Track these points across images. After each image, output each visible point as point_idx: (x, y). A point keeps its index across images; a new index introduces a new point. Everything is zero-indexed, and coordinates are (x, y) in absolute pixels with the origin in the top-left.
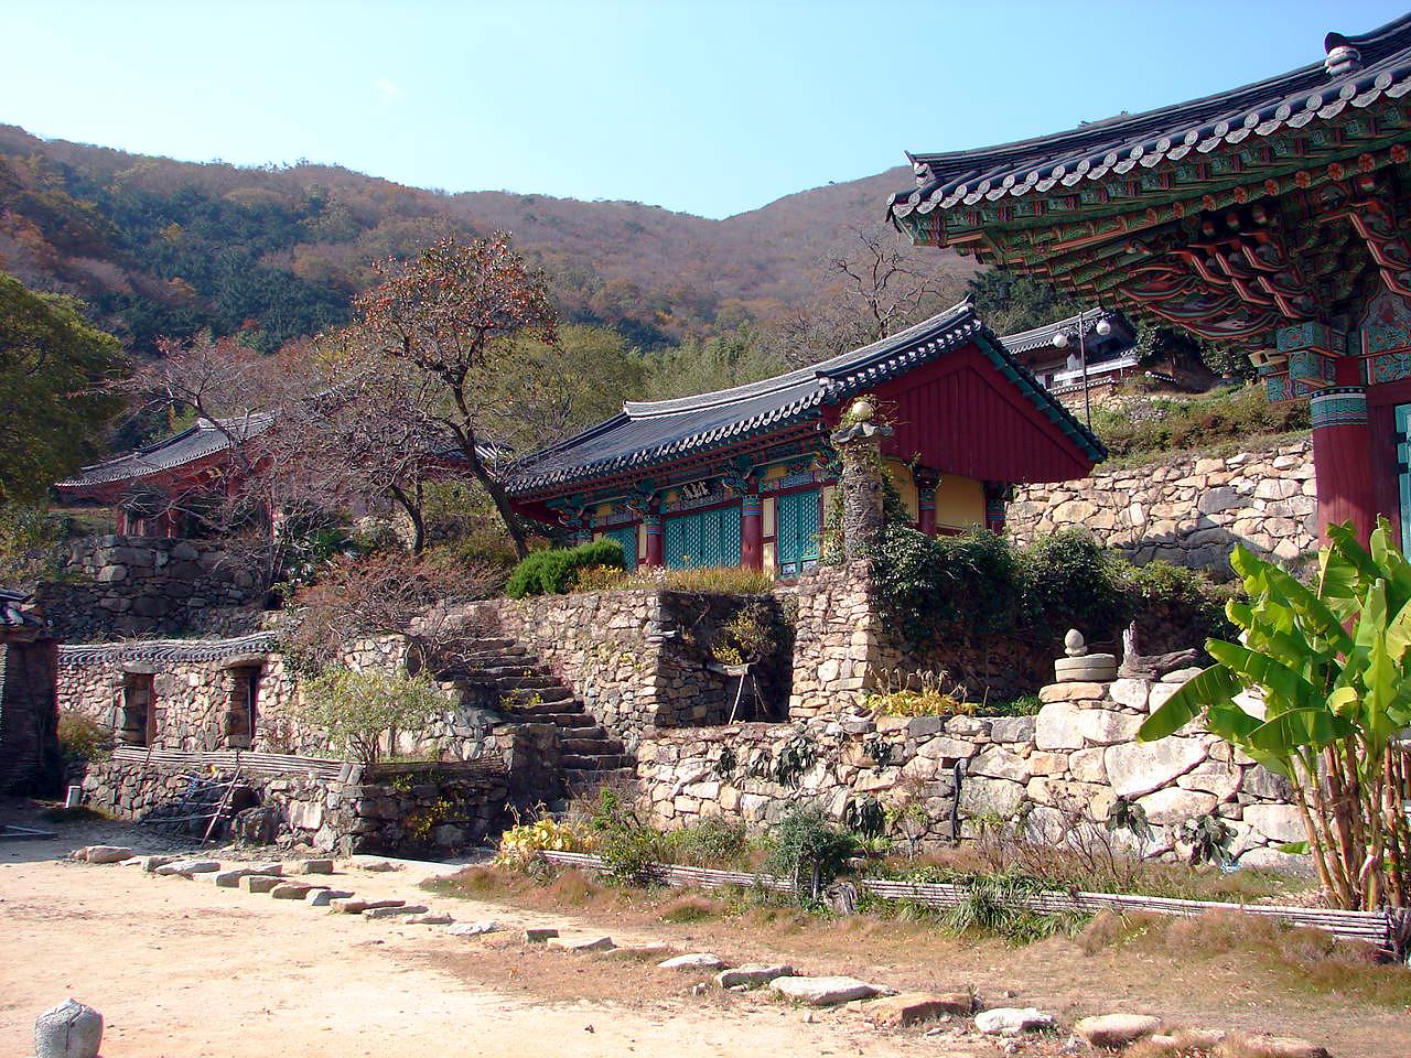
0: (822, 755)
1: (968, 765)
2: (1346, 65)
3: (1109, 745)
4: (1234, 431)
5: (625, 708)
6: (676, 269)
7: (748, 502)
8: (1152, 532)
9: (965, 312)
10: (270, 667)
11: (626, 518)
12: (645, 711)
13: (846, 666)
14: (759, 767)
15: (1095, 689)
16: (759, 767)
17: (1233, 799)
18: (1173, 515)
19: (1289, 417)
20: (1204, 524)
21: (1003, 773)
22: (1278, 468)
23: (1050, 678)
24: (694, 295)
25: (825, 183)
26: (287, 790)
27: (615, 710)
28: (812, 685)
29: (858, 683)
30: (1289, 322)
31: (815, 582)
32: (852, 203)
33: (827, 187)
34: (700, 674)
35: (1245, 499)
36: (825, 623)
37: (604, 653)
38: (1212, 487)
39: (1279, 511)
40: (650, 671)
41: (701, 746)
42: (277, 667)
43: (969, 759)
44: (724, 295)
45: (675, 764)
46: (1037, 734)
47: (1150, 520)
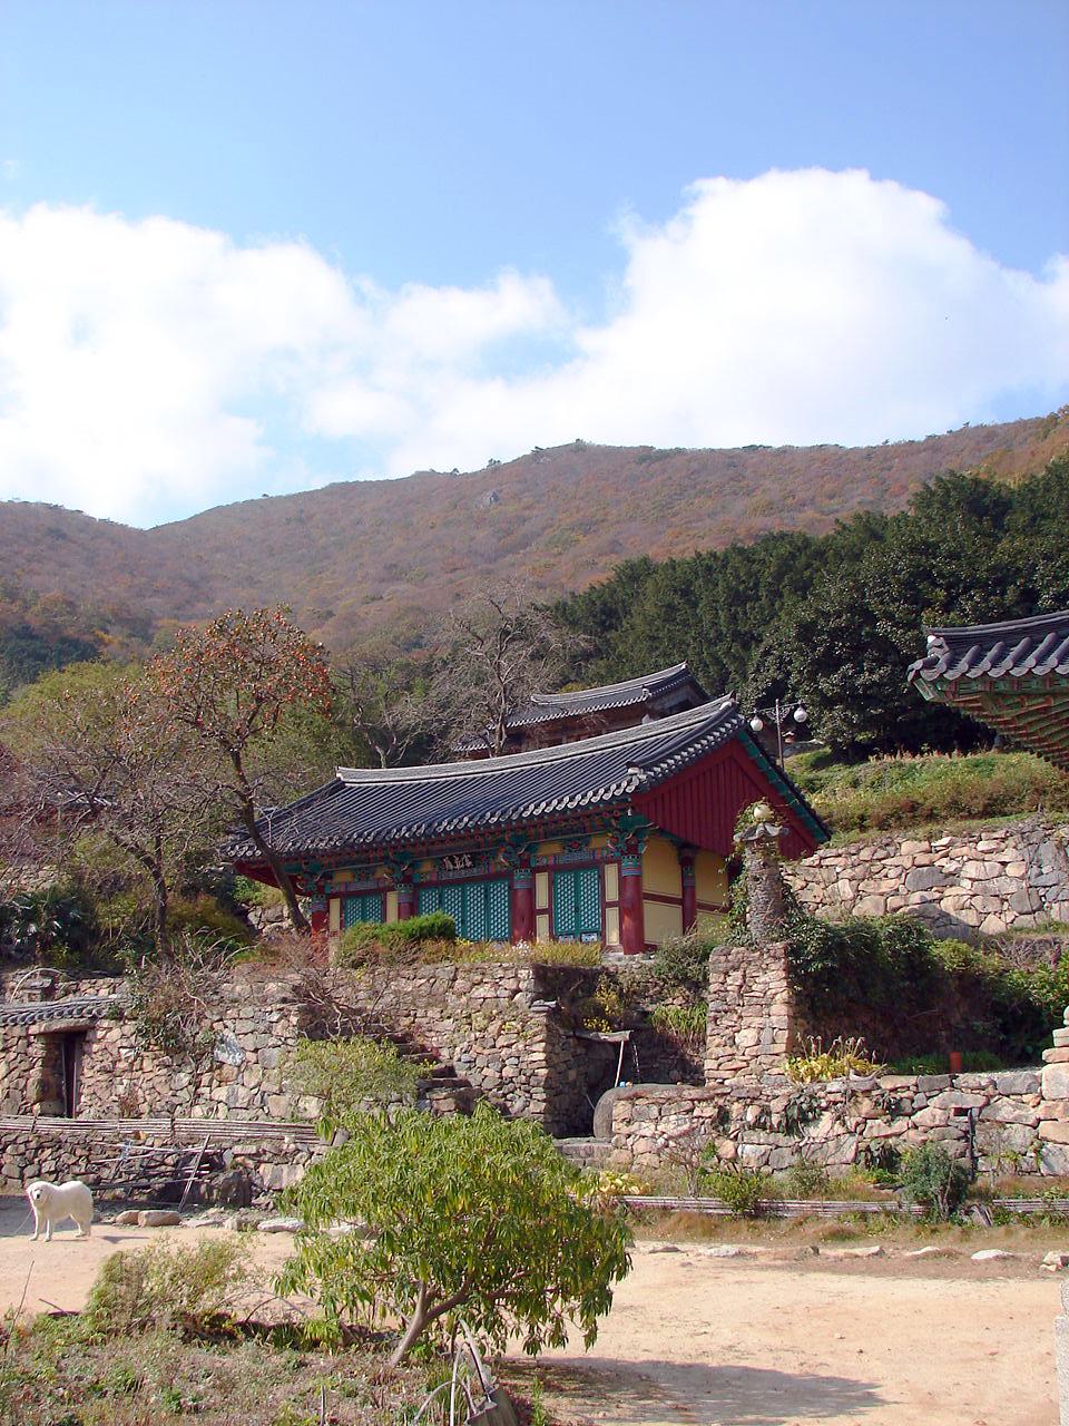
0: (826, 1109)
1: (980, 1113)
4: (931, 816)
5: (508, 1072)
6: (105, 583)
7: (520, 876)
9: (728, 708)
10: (100, 1034)
11: (370, 885)
12: (533, 1074)
13: (766, 1035)
14: (762, 1120)
16: (762, 1120)
18: (881, 891)
19: (986, 806)
21: (1015, 1118)
22: (982, 852)
23: (1051, 1045)
24: (128, 611)
25: (258, 496)
26: (257, 1154)
27: (498, 1075)
28: (729, 1050)
29: (780, 1048)
32: (289, 521)
33: (261, 500)
34: (571, 1040)
35: (952, 878)
36: (741, 996)
37: (479, 1021)
38: (918, 867)
39: (985, 889)
40: (538, 1038)
41: (688, 1105)
42: (113, 1037)
43: (981, 1109)
44: (158, 614)
45: (657, 1121)
46: (1044, 1087)
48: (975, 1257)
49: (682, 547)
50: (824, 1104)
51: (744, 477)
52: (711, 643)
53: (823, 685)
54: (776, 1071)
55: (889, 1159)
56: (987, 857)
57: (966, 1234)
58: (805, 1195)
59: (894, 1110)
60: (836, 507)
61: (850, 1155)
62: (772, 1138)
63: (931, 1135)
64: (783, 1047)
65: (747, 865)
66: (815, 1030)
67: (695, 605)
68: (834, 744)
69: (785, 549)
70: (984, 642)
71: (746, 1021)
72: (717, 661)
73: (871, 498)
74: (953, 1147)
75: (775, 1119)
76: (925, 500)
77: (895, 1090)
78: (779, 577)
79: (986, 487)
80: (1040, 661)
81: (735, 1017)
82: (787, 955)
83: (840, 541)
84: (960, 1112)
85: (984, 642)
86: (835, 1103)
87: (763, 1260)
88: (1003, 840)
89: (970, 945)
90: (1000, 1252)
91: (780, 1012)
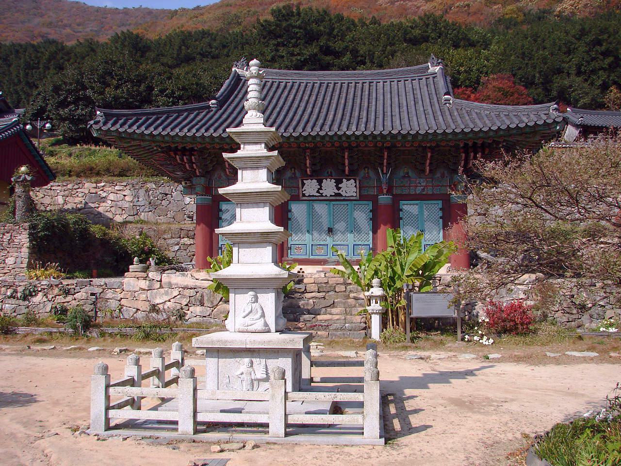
0: (40, 291)
2: (216, 106)
3: (148, 290)
4: (98, 174)
8: (66, 207)
9: (16, 121)
13: (19, 260)
15: (144, 275)
17: (187, 305)
19: (120, 172)
20: (87, 206)
23: (128, 271)
30: (198, 176)
31: (4, 229)
35: (104, 199)
36: (9, 244)
39: (116, 205)
47: (65, 202)
48: (89, 350)
49: (7, 34)
50: (40, 289)
51: (40, 8)
52: (15, 85)
53: (61, 113)
54: (22, 274)
55: (64, 311)
56: (118, 192)
57: (89, 340)
58: (28, 325)
59: (67, 293)
60: (81, 30)
61: (48, 309)
62: (17, 302)
63: (82, 302)
64: (26, 265)
65: (16, 190)
66: (39, 259)
67: (10, 66)
68: (63, 135)
69: (53, 49)
70: (119, 117)
71: (11, 254)
72: (17, 92)
73: (96, 29)
74: (88, 308)
75: (19, 295)
76: (116, 39)
77: (68, 285)
78: (49, 60)
79: (141, 39)
80: (138, 128)
81: (6, 252)
82: (30, 229)
83: (78, 50)
84: (92, 294)
85: (119, 117)
86: (44, 289)
87: (7, 351)
88: (125, 186)
89: (107, 228)
90: (98, 348)
91: (25, 251)
